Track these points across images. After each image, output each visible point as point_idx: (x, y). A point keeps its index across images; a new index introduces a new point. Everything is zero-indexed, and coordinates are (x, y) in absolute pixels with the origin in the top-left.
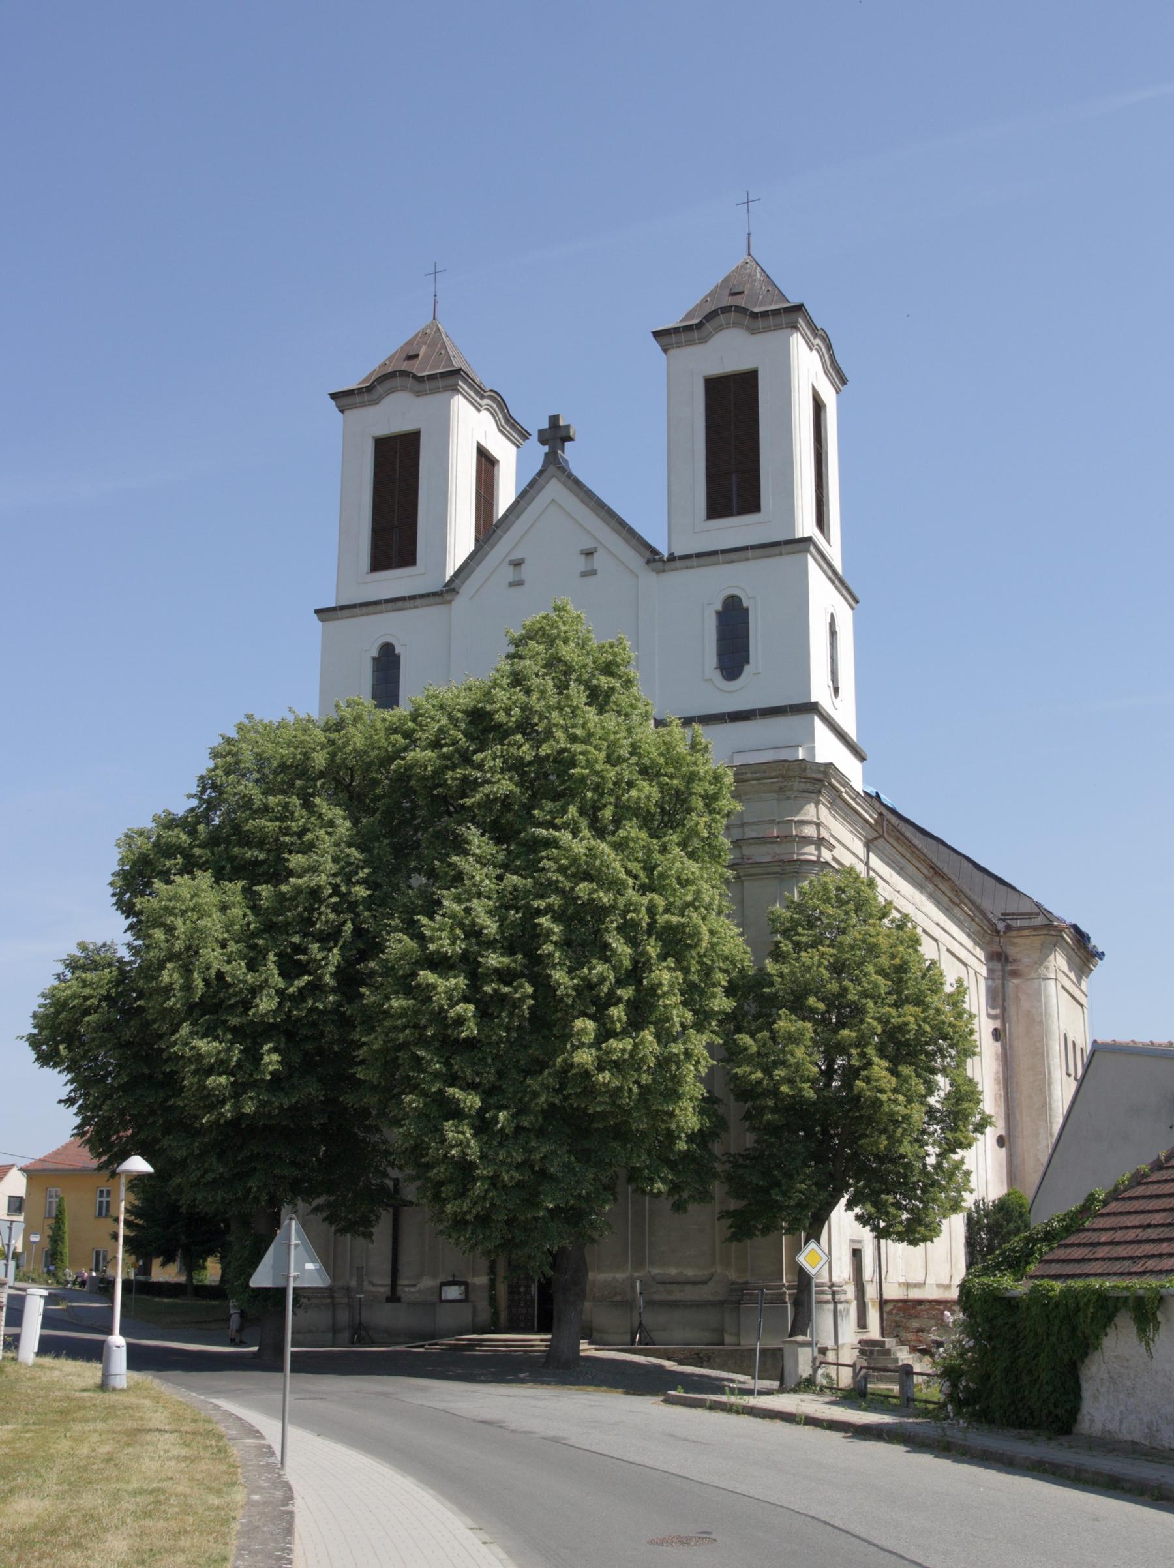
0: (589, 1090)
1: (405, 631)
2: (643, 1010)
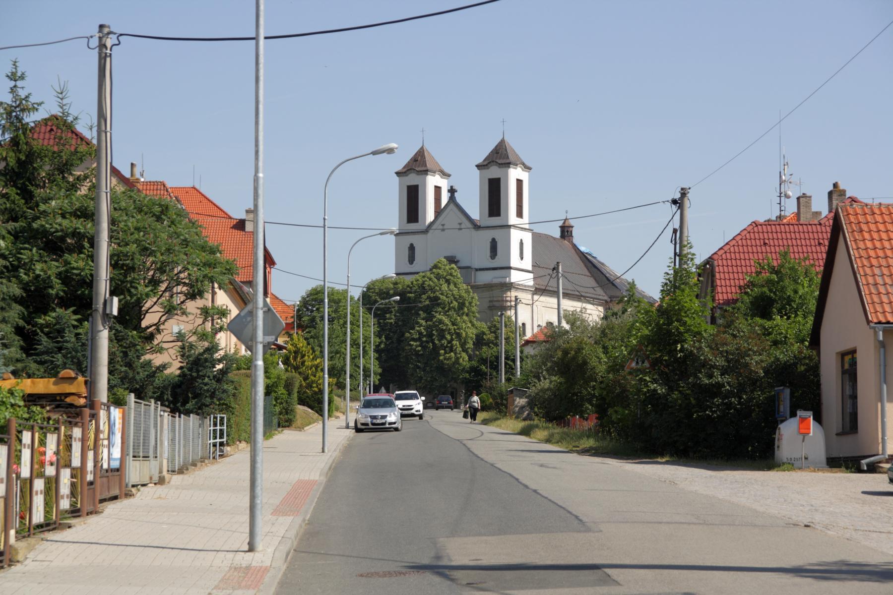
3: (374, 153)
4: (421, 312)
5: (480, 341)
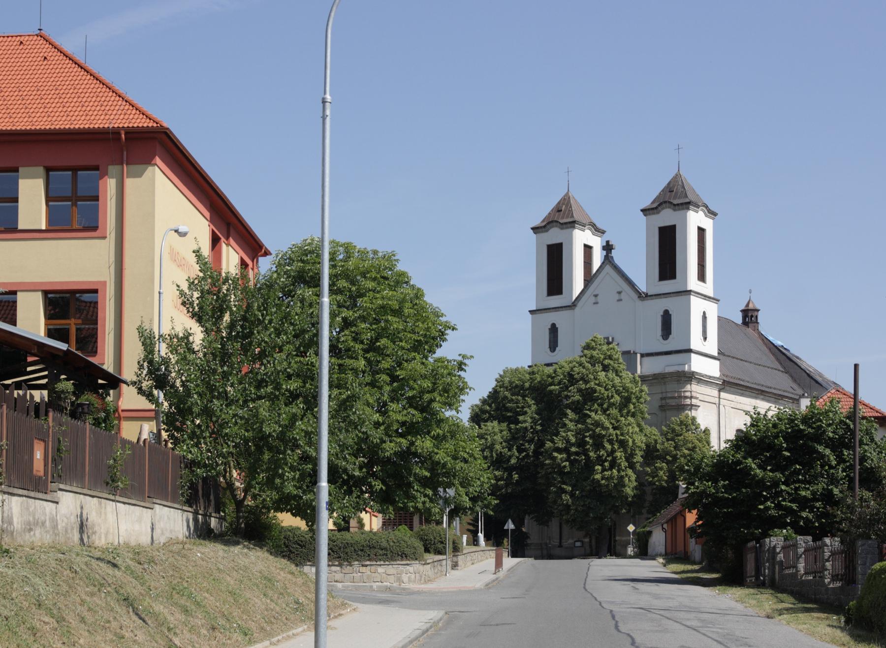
0: (600, 485)
1: (561, 319)
2: (614, 464)
4: (569, 411)
5: (651, 454)
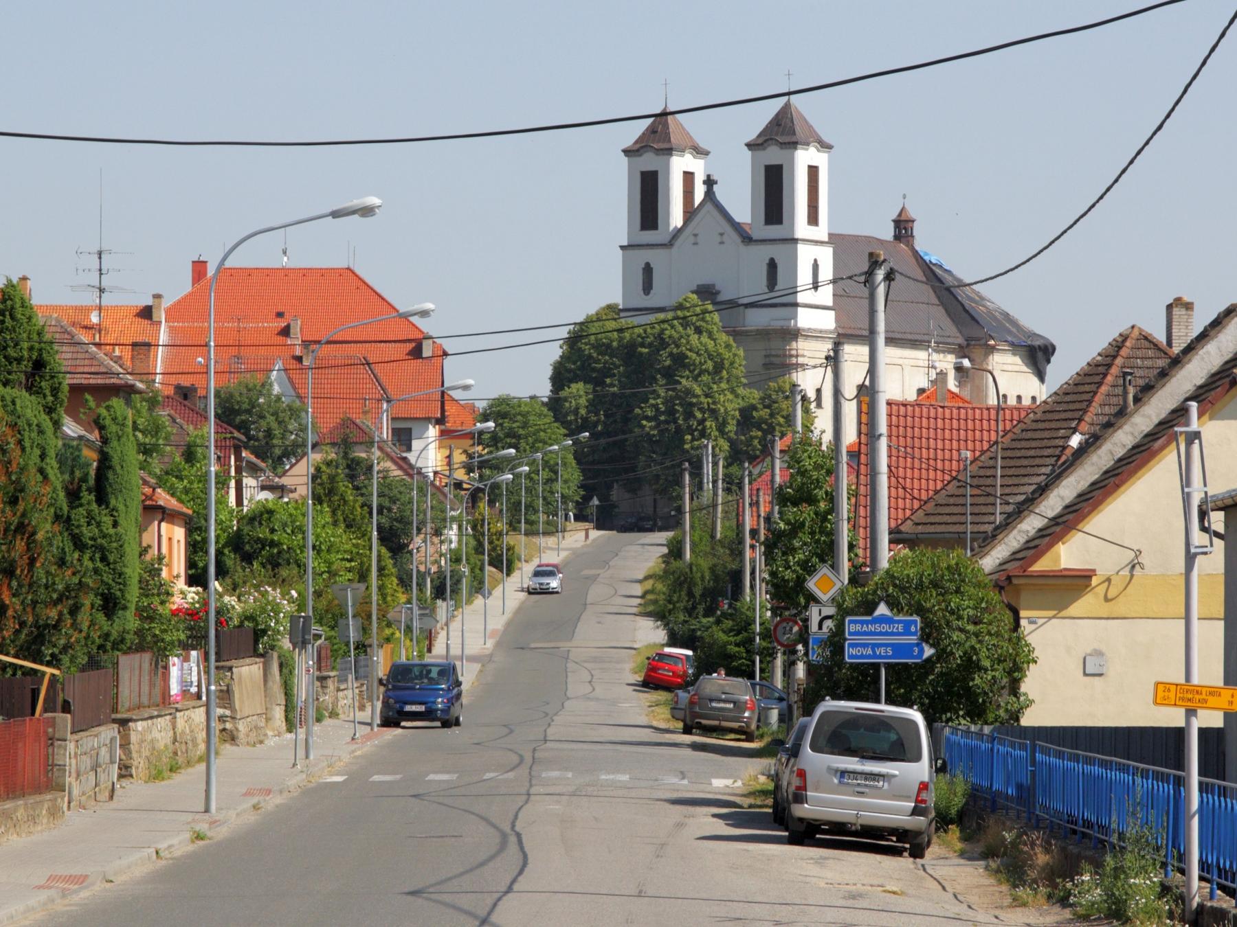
3: (336, 214)
